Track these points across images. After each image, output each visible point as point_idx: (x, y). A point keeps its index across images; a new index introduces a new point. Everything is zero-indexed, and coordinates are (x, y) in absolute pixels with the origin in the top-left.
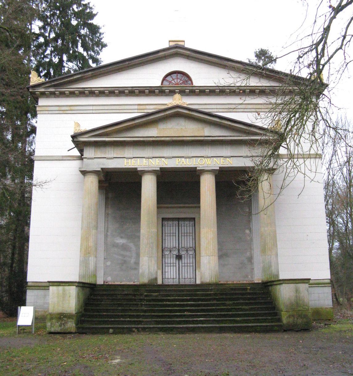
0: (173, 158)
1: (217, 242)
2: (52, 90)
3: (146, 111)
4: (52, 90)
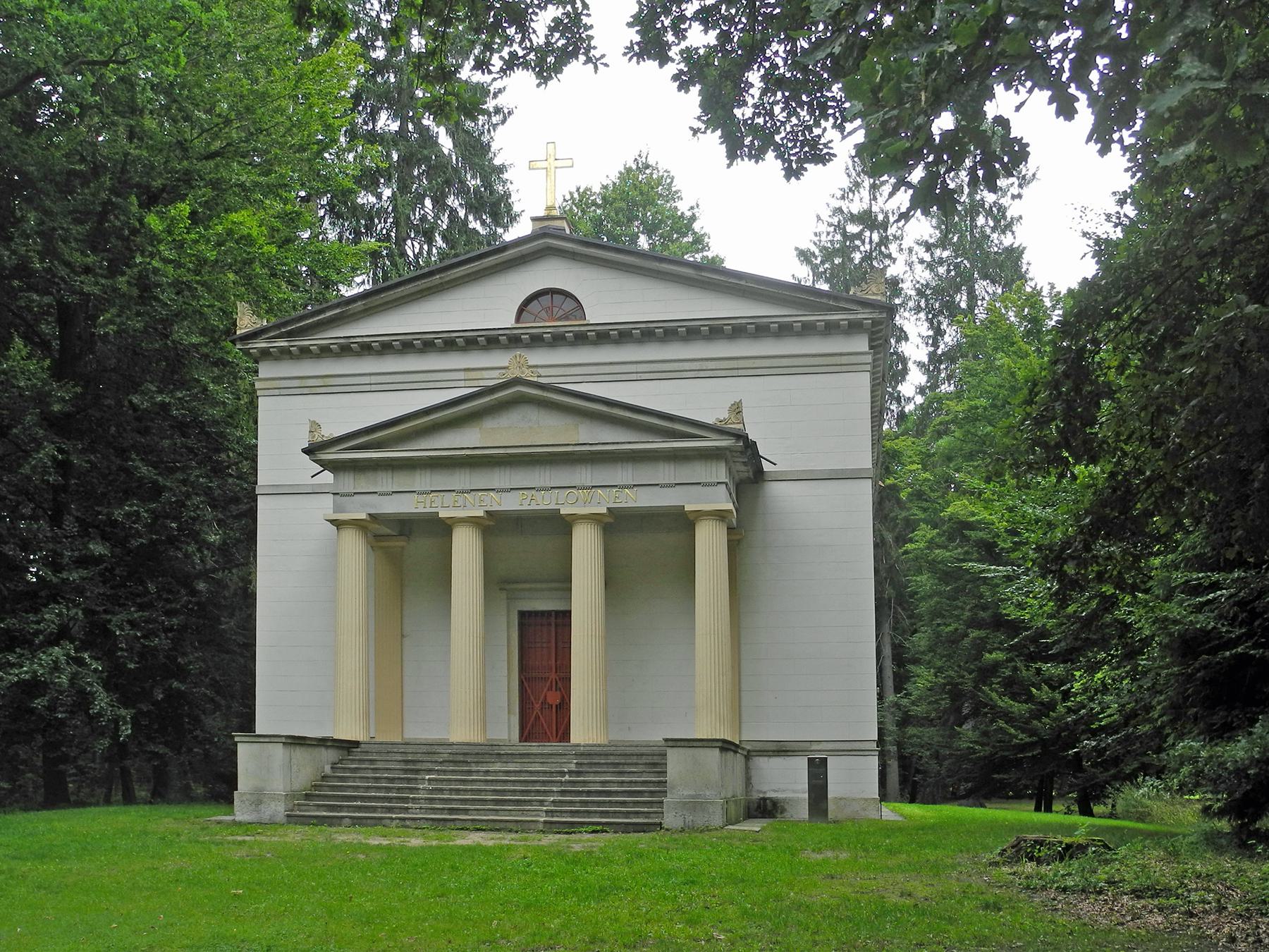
0: (395, 496)
1: (45, 814)
2: (282, 343)
3: (482, 383)
4: (282, 343)
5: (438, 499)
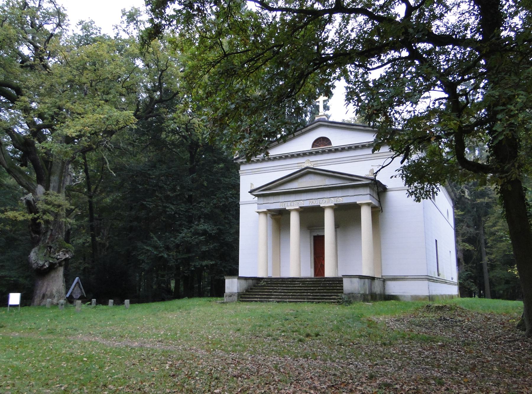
5: (286, 204)
